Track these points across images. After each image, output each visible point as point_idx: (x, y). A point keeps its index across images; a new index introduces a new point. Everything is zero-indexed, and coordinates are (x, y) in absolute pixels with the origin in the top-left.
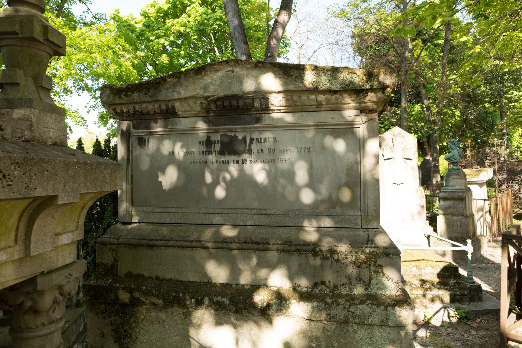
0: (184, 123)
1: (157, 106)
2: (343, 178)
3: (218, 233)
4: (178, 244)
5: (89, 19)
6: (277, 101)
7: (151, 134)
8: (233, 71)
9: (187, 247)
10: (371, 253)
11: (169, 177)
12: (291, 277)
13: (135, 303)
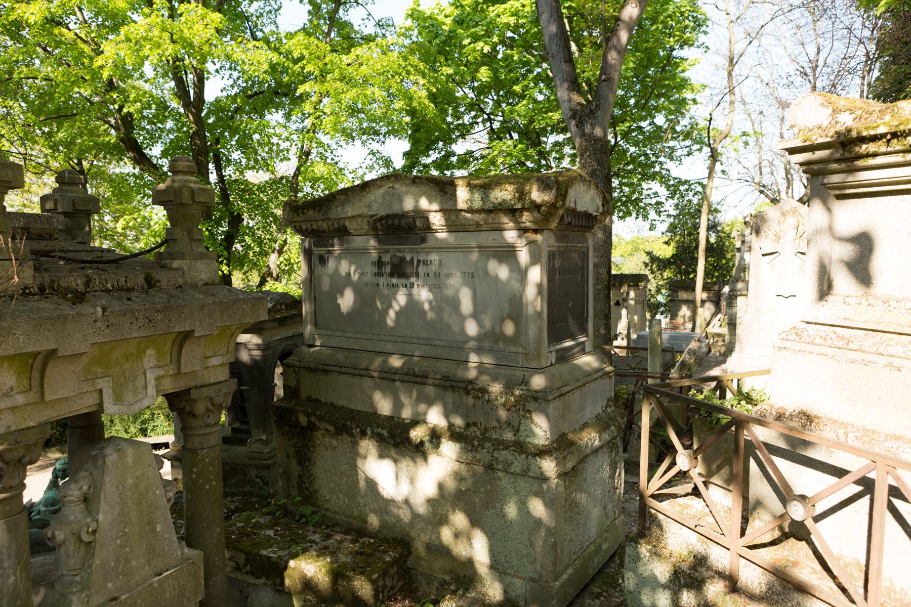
0: (357, 242)
1: (330, 224)
2: (506, 309)
3: (385, 362)
4: (349, 371)
5: (370, 29)
6: (437, 220)
7: (330, 252)
8: (393, 188)
9: (356, 375)
10: (520, 396)
11: (347, 301)
12: (447, 416)
13: (312, 427)
